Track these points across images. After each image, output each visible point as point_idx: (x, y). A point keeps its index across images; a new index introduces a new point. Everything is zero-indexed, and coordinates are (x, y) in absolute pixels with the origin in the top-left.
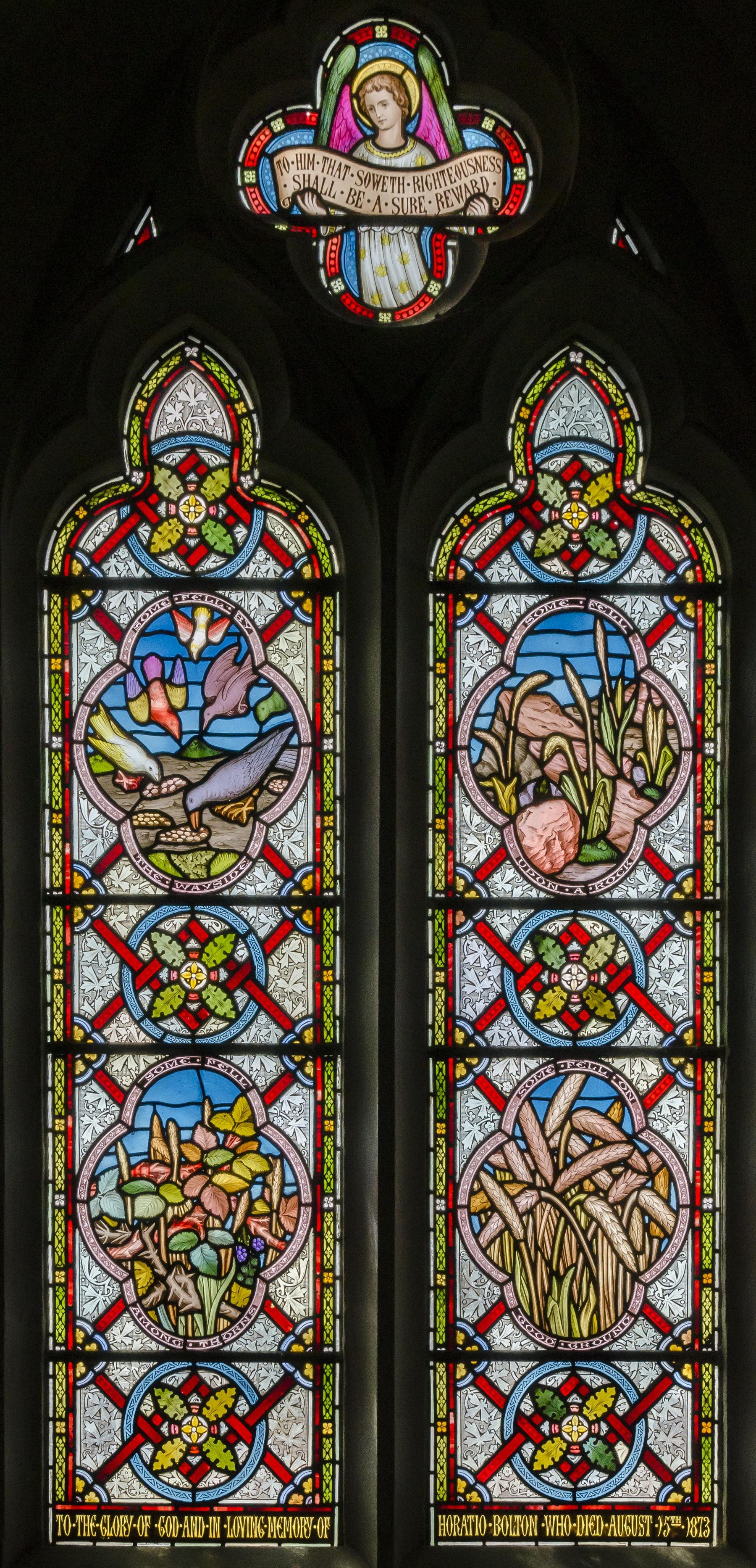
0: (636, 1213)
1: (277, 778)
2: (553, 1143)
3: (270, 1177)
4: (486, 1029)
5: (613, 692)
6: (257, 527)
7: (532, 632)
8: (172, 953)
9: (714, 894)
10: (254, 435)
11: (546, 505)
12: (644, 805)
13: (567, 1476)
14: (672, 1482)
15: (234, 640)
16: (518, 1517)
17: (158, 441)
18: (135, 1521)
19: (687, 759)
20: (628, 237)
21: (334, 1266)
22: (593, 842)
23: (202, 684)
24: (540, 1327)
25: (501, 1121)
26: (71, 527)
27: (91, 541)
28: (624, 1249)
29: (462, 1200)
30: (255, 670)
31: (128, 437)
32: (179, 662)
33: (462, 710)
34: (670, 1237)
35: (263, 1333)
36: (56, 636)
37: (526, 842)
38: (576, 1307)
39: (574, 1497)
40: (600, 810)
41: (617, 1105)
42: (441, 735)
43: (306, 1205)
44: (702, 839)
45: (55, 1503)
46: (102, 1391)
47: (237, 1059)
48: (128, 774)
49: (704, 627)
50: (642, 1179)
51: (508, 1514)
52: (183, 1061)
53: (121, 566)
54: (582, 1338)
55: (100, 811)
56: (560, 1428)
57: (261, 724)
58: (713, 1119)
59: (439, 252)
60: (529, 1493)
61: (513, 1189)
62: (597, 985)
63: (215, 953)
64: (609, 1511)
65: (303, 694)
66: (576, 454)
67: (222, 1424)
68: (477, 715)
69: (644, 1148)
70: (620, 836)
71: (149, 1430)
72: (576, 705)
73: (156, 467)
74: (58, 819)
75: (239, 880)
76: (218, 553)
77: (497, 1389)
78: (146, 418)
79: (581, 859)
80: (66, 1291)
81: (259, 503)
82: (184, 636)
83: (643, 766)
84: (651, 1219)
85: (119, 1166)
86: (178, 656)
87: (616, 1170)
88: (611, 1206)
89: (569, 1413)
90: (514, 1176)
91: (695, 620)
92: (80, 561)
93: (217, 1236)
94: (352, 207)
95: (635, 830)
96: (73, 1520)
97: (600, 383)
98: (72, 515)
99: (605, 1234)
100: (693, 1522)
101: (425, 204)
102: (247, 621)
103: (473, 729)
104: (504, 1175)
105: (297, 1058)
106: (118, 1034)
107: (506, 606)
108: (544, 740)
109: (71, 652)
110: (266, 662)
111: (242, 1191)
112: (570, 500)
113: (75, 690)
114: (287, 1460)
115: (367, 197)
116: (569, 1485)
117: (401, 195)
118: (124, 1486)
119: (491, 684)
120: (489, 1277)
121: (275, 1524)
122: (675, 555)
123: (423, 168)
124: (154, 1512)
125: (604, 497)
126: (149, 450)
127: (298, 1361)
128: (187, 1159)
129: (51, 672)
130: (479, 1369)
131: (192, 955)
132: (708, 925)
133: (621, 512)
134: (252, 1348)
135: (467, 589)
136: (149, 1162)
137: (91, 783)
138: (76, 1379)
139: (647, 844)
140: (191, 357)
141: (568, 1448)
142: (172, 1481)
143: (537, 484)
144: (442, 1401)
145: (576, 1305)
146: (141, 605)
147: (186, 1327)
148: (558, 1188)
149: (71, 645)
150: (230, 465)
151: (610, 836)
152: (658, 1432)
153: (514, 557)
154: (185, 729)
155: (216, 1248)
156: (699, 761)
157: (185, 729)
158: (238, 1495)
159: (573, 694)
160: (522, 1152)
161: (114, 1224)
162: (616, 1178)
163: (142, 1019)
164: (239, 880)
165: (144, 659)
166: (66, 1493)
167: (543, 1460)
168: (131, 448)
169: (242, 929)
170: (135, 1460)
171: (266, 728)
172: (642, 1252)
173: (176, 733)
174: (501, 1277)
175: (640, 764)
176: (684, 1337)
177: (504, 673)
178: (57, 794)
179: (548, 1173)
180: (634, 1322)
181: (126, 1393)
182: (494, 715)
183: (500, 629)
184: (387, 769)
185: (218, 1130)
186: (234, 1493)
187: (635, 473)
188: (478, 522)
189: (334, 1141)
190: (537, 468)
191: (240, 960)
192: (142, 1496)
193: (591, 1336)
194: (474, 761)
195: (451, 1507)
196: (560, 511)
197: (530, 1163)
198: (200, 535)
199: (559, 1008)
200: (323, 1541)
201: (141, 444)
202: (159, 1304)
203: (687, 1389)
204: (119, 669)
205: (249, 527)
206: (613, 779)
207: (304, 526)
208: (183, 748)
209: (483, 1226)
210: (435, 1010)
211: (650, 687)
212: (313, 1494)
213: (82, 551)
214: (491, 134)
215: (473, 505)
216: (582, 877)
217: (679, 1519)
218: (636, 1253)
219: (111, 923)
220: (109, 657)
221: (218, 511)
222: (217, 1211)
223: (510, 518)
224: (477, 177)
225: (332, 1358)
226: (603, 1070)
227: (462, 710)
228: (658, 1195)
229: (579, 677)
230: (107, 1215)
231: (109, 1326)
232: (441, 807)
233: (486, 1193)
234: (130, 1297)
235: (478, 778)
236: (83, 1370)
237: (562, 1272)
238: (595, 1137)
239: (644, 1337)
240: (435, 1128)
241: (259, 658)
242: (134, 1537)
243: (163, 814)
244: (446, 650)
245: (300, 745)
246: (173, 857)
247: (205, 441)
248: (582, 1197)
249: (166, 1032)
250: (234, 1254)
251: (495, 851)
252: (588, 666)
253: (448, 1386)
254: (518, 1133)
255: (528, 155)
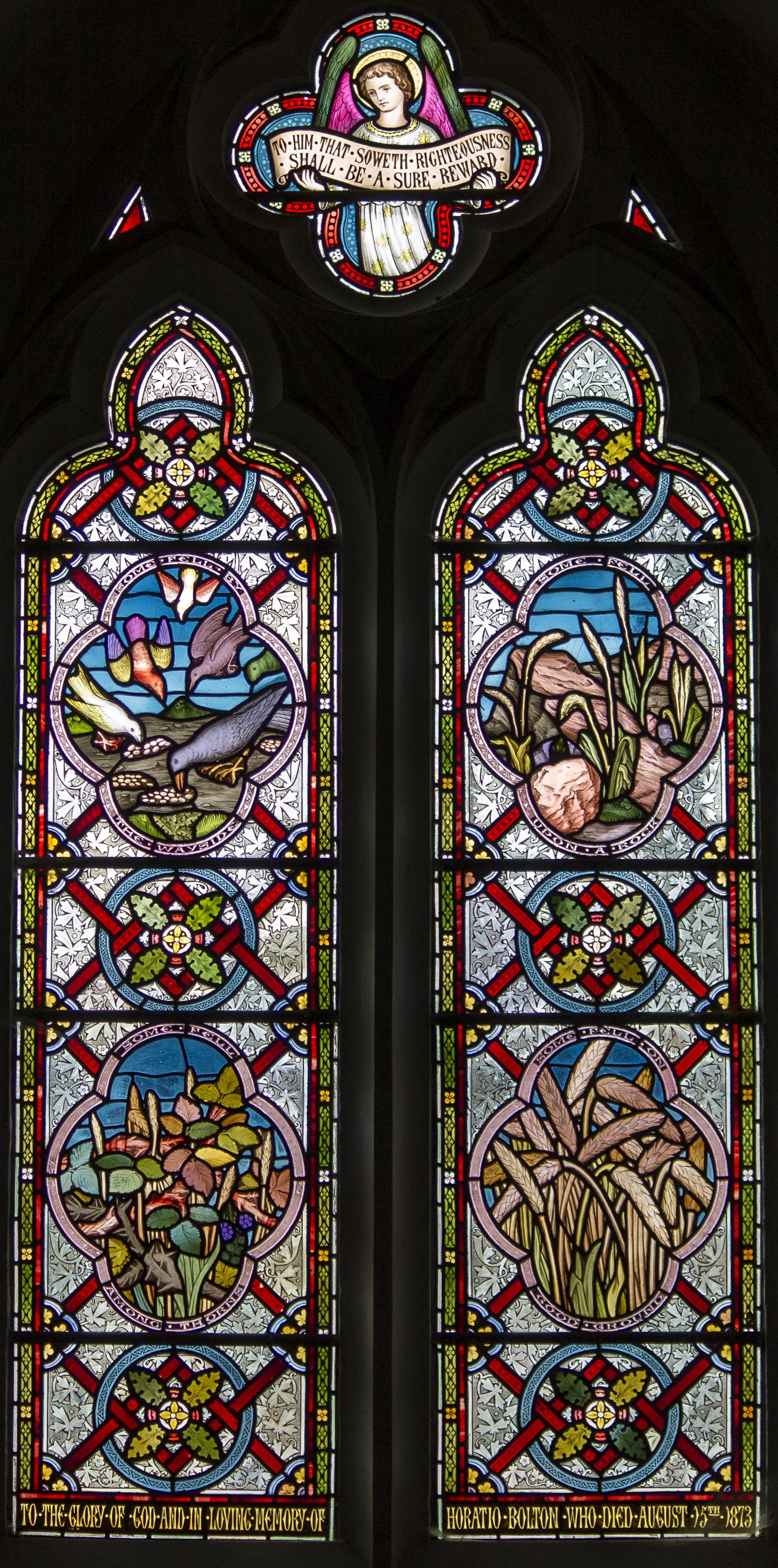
0: (669, 1185)
1: (269, 738)
2: (575, 1111)
3: (258, 1152)
4: (500, 994)
5: (636, 650)
6: (249, 489)
7: (546, 590)
8: (154, 917)
9: (749, 853)
10: (247, 400)
11: (561, 463)
12: (672, 763)
13: (591, 1465)
14: (710, 1470)
15: (224, 600)
16: (536, 1509)
17: (144, 407)
18: (107, 1511)
19: (718, 715)
20: (645, 209)
21: (330, 1244)
22: (616, 801)
23: (189, 644)
24: (562, 1307)
25: (517, 1088)
26: (51, 491)
27: (72, 505)
28: (656, 1222)
29: (475, 1170)
30: (246, 630)
31: (113, 404)
32: (164, 622)
33: (471, 669)
34: (707, 1210)
35: (251, 1314)
36: (33, 598)
37: (542, 802)
38: (602, 1284)
39: (600, 1488)
40: (622, 769)
41: (646, 1072)
42: (448, 693)
43: (300, 1179)
44: (736, 797)
45: (18, 1493)
46: (71, 1374)
47: (223, 1027)
48: (108, 735)
49: (733, 583)
50: (676, 1149)
51: (525, 1505)
52: (165, 1028)
53: (103, 529)
54: (609, 1318)
55: (78, 772)
56: (584, 1414)
57: (252, 684)
58: (753, 1087)
59: (444, 223)
60: (549, 1483)
61: (532, 1159)
62: (622, 947)
63: (200, 917)
64: (638, 1502)
65: (298, 654)
66: (592, 413)
67: (205, 1410)
68: (488, 672)
69: (678, 1117)
70: (645, 795)
71: (122, 1416)
72: (596, 662)
73: (142, 432)
74: (32, 780)
75: (227, 841)
76: (207, 515)
77: (514, 1373)
78: (133, 386)
79: (602, 818)
80: (33, 1270)
81: (252, 465)
82: (171, 597)
83: (670, 723)
84: (686, 1191)
85: (93, 1139)
86: (163, 617)
87: (645, 1140)
88: (641, 1177)
89: (594, 1398)
90: (533, 1145)
91: (723, 577)
92: (60, 525)
93: (201, 1213)
94: (352, 183)
95: (662, 789)
96: (40, 1509)
97: (617, 345)
98: (53, 479)
99: (635, 1206)
100: (732, 1512)
101: (429, 178)
102: (238, 582)
103: (483, 686)
104: (523, 1148)
105: (290, 1026)
106: (94, 1001)
107: (518, 564)
108: (561, 698)
109: (49, 614)
110: (258, 622)
111: (228, 1166)
112: (587, 457)
113: (52, 651)
114: (277, 1448)
115: (368, 173)
116: (594, 1475)
117: (403, 171)
118: (95, 1474)
119: (502, 643)
120: (505, 1254)
121: (262, 1516)
122: (701, 512)
123: (427, 145)
124: (128, 1501)
125: (623, 456)
126: (135, 416)
127: (290, 1343)
128: (167, 1132)
129: (27, 633)
130: (492, 1352)
131: (175, 919)
132: (743, 885)
133: (642, 470)
134: (238, 1330)
135: (477, 551)
136: (126, 1135)
137: (69, 744)
138: (43, 1362)
139: (675, 802)
140: (181, 326)
141: (593, 1435)
142: (148, 1470)
143: (550, 442)
144: (451, 1386)
145: (602, 1285)
146: (124, 567)
147: (165, 1308)
148: (582, 1157)
149: (49, 607)
150: (221, 429)
151: (633, 796)
152: (694, 1417)
153: (525, 515)
154: (170, 689)
155: (199, 1225)
156: (731, 718)
157: (170, 689)
158: (222, 1485)
159: (592, 652)
160: (541, 1120)
161: (86, 1200)
162: (646, 1147)
163: (120, 985)
164: (227, 841)
165: (127, 620)
166: (31, 1481)
167: (565, 1448)
168: (116, 414)
169: (231, 891)
170: (108, 1447)
171: (257, 688)
172: (677, 1226)
173: (161, 694)
174: (518, 1254)
175: (667, 721)
176: (723, 1316)
177: (516, 632)
178: (31, 755)
179: (571, 1140)
180: (667, 1301)
181: (99, 1376)
182: (505, 673)
183: (512, 587)
184: (387, 724)
185: (202, 1101)
186: (218, 1482)
187: (656, 431)
188: (487, 481)
189: (331, 1112)
190: (550, 427)
191: (228, 923)
192: (116, 1485)
193: (618, 1316)
194: (485, 717)
195: (461, 1499)
196: (576, 469)
197: (551, 1132)
198: (187, 497)
199: (580, 972)
200: (317, 1534)
201: (127, 410)
202: (135, 1284)
203: (726, 1372)
204: (99, 631)
205: (241, 489)
206: (637, 738)
207: (299, 488)
208: (167, 709)
209: (497, 1200)
210: (441, 975)
211: (675, 643)
212: (305, 1485)
213: (62, 514)
214: (499, 113)
215: (482, 464)
216: (604, 837)
217: (717, 1509)
218: (669, 1227)
219: (88, 886)
220: (90, 619)
221: (208, 473)
222: (201, 1187)
223: (522, 476)
224: (484, 153)
225: (327, 1341)
226: (630, 1036)
227: (471, 669)
228: (693, 1165)
229: (598, 636)
230: (79, 1190)
231: (81, 1306)
232: (448, 768)
233: (501, 1164)
234: (104, 1276)
235: (489, 736)
236: (51, 1352)
237: (586, 1248)
238: (622, 1105)
239: (678, 1316)
240: (443, 1097)
241: (250, 617)
242: (106, 1527)
243: (145, 775)
244: (453, 608)
245: (295, 704)
246: (156, 819)
247: (195, 407)
248: (609, 1167)
249: (147, 998)
250: (219, 1231)
251: (508, 811)
252: (607, 623)
253: (458, 1370)
254: (537, 1101)
255: (537, 133)
